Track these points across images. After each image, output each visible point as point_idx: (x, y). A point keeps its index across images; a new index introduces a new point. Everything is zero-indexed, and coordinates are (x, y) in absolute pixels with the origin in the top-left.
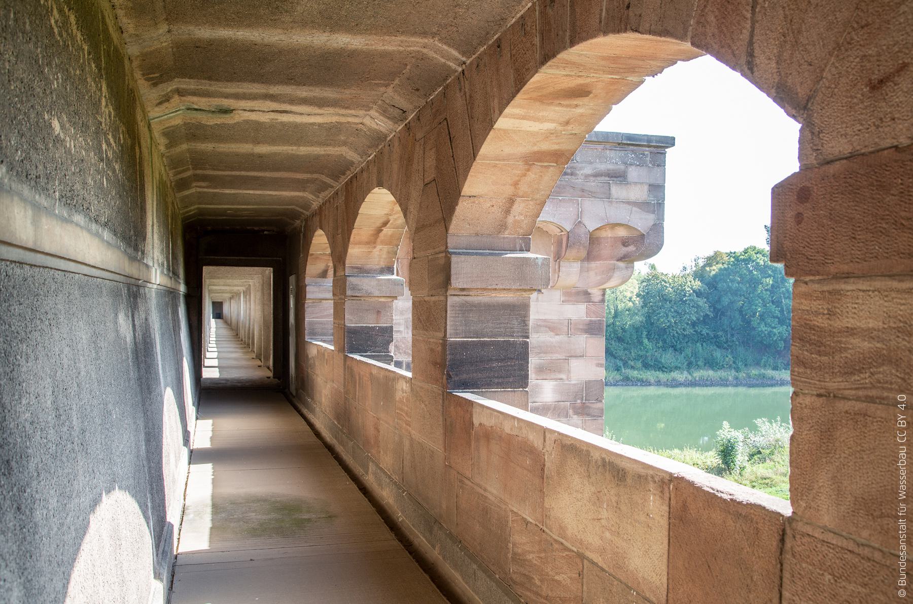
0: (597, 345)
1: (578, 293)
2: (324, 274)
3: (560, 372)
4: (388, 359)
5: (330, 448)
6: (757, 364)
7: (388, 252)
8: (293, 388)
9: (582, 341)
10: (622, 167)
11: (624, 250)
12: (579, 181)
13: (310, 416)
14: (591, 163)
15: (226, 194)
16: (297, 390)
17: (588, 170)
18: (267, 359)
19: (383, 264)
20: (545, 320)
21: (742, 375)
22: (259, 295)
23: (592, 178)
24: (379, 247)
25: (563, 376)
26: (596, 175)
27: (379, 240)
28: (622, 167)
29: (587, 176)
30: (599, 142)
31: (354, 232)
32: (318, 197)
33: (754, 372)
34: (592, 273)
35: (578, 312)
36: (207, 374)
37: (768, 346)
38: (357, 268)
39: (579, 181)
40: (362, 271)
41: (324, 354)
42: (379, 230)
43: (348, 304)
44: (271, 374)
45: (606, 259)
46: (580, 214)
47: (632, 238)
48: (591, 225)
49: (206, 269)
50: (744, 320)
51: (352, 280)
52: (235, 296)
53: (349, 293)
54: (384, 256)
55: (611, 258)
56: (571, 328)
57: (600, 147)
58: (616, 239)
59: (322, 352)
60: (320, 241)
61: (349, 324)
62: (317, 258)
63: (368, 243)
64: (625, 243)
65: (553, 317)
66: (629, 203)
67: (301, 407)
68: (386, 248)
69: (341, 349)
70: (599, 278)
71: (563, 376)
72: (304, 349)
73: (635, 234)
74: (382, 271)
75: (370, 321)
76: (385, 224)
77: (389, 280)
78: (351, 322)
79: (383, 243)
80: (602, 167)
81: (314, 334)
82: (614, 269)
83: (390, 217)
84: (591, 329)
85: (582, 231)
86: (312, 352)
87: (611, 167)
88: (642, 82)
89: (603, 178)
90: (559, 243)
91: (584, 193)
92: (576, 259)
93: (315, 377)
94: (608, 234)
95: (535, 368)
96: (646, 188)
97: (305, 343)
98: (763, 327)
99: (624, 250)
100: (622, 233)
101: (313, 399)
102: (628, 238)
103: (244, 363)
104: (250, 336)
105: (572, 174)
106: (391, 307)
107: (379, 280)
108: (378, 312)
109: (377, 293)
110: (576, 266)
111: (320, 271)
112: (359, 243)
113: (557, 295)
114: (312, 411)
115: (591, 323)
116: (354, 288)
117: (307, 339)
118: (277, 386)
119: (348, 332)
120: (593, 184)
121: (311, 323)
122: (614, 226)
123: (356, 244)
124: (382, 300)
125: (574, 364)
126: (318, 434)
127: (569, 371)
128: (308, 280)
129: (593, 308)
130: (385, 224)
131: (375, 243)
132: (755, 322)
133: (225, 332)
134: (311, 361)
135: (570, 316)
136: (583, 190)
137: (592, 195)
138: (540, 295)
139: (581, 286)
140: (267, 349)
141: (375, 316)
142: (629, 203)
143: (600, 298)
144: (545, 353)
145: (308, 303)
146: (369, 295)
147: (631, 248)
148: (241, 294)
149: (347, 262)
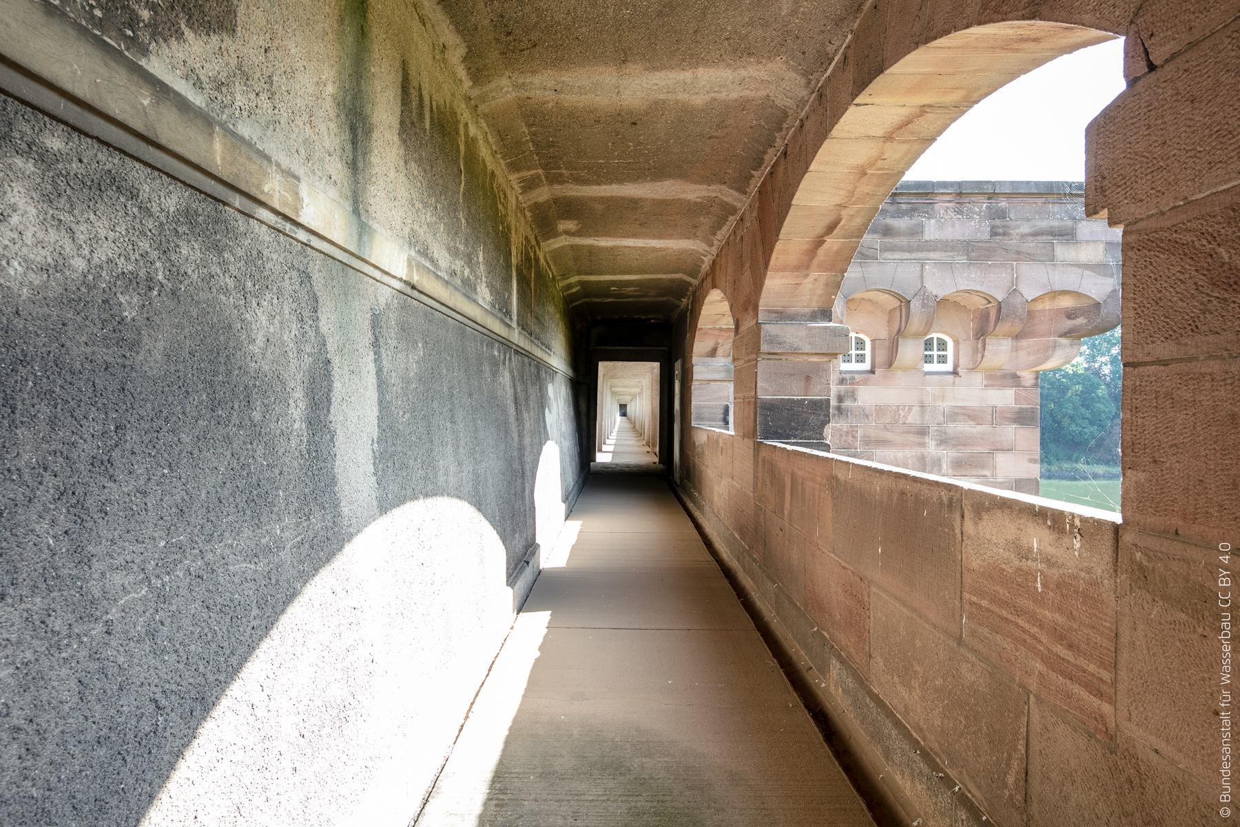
0: (1030, 438)
1: (1004, 376)
2: (713, 353)
3: (983, 467)
4: (827, 448)
5: (728, 573)
6: (1069, 459)
7: (827, 285)
8: (677, 476)
9: (1010, 432)
10: (1070, 223)
11: (1070, 323)
12: (1013, 242)
13: (697, 514)
14: (1028, 220)
15: (601, 249)
16: (681, 479)
17: (1025, 229)
18: (654, 446)
19: (815, 306)
20: (963, 408)
21: (1054, 468)
22: (649, 392)
23: (1030, 238)
24: (814, 275)
25: (987, 473)
26: (1035, 234)
27: (815, 262)
28: (1070, 223)
29: (1023, 236)
30: (1040, 195)
31: (779, 246)
32: (711, 245)
33: (1066, 465)
34: (1022, 353)
35: (1005, 398)
36: (603, 457)
37: (1080, 444)
38: (776, 312)
39: (1013, 242)
40: (782, 316)
41: (717, 441)
42: (819, 242)
43: (762, 366)
44: (657, 460)
45: (1042, 336)
46: (1015, 281)
47: (1080, 309)
48: (1029, 293)
49: (603, 366)
50: (1054, 421)
51: (769, 329)
52: (634, 396)
53: (764, 348)
54: (819, 292)
55: (1049, 334)
56: (998, 416)
57: (1040, 201)
58: (1058, 312)
59: (714, 440)
60: (715, 310)
61: (762, 396)
62: (706, 333)
63: (797, 268)
64: (1070, 315)
65: (972, 403)
66: (1079, 266)
67: (691, 505)
68: (824, 276)
69: (749, 434)
70: (1032, 358)
71: (987, 473)
72: (690, 437)
73: (1085, 303)
74: (814, 317)
75: (794, 392)
76: (831, 229)
77: (825, 328)
78: (767, 391)
79: (822, 267)
80: (1044, 224)
81: (700, 419)
82: (1055, 346)
83: (844, 213)
84: (1021, 418)
85: (1018, 300)
86: (700, 438)
87: (1055, 224)
88: (512, 579)
89: (1045, 237)
90: (983, 317)
91: (1020, 255)
92: (1005, 336)
93: (703, 468)
94: (1047, 305)
95: (952, 462)
96: (1101, 247)
97: (691, 428)
98: (1073, 427)
99: (1070, 323)
100: (1066, 303)
101: (700, 493)
102: (1075, 309)
103: (636, 449)
104: (643, 427)
105: (1004, 234)
106: (826, 371)
107: (810, 329)
108: (808, 378)
109: (807, 349)
110: (1006, 345)
111: (709, 349)
112: (783, 269)
113: (978, 378)
114: (700, 508)
115: (1021, 411)
116: (772, 340)
117: (694, 424)
118: (665, 478)
119: (762, 408)
120: (1030, 245)
121: (699, 407)
122: (1055, 294)
123: (778, 270)
124: (815, 359)
125: (1001, 458)
126: (708, 544)
127: (994, 468)
128: (695, 360)
129: (1023, 393)
130: (831, 229)
131: (808, 267)
132: (1066, 422)
133: (627, 425)
134: (699, 449)
135: (994, 403)
136: (1018, 253)
137: (1031, 257)
138: (957, 379)
139: (1009, 368)
140: (654, 438)
141: (802, 384)
142: (1079, 266)
143: (1033, 381)
144: (964, 445)
145: (695, 386)
146: (795, 352)
147: (1081, 321)
148: (629, 388)
149: (762, 302)
